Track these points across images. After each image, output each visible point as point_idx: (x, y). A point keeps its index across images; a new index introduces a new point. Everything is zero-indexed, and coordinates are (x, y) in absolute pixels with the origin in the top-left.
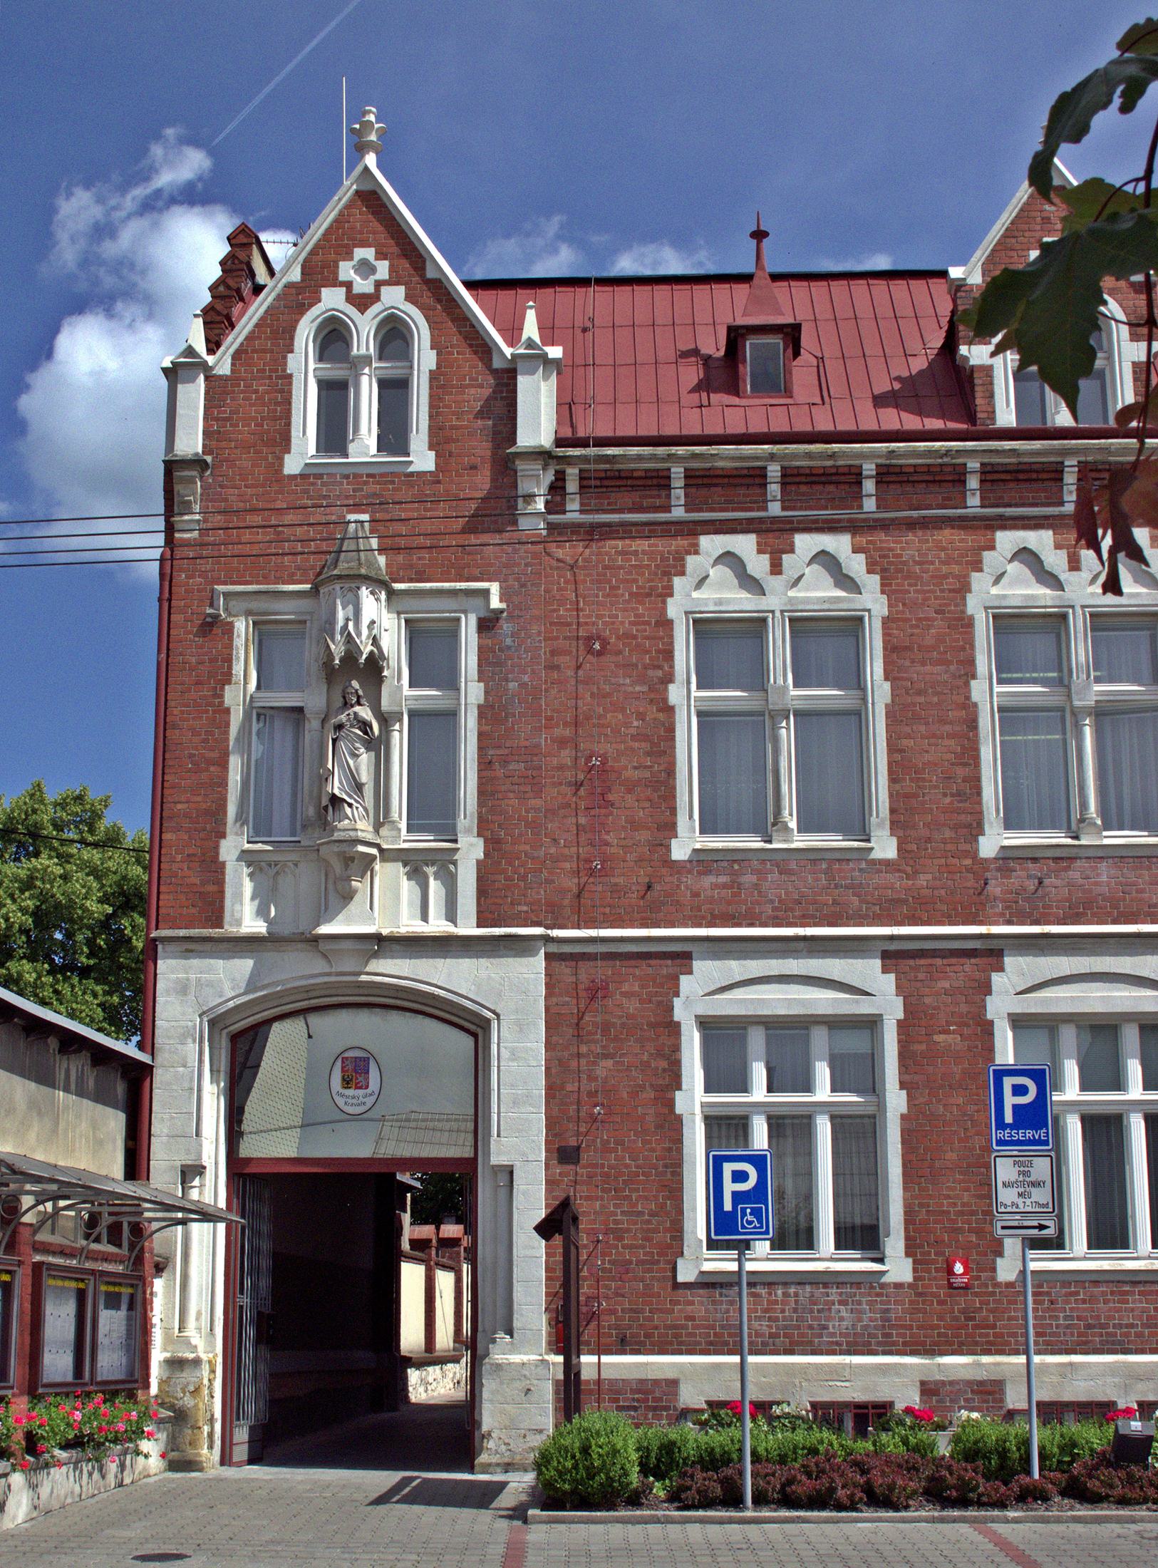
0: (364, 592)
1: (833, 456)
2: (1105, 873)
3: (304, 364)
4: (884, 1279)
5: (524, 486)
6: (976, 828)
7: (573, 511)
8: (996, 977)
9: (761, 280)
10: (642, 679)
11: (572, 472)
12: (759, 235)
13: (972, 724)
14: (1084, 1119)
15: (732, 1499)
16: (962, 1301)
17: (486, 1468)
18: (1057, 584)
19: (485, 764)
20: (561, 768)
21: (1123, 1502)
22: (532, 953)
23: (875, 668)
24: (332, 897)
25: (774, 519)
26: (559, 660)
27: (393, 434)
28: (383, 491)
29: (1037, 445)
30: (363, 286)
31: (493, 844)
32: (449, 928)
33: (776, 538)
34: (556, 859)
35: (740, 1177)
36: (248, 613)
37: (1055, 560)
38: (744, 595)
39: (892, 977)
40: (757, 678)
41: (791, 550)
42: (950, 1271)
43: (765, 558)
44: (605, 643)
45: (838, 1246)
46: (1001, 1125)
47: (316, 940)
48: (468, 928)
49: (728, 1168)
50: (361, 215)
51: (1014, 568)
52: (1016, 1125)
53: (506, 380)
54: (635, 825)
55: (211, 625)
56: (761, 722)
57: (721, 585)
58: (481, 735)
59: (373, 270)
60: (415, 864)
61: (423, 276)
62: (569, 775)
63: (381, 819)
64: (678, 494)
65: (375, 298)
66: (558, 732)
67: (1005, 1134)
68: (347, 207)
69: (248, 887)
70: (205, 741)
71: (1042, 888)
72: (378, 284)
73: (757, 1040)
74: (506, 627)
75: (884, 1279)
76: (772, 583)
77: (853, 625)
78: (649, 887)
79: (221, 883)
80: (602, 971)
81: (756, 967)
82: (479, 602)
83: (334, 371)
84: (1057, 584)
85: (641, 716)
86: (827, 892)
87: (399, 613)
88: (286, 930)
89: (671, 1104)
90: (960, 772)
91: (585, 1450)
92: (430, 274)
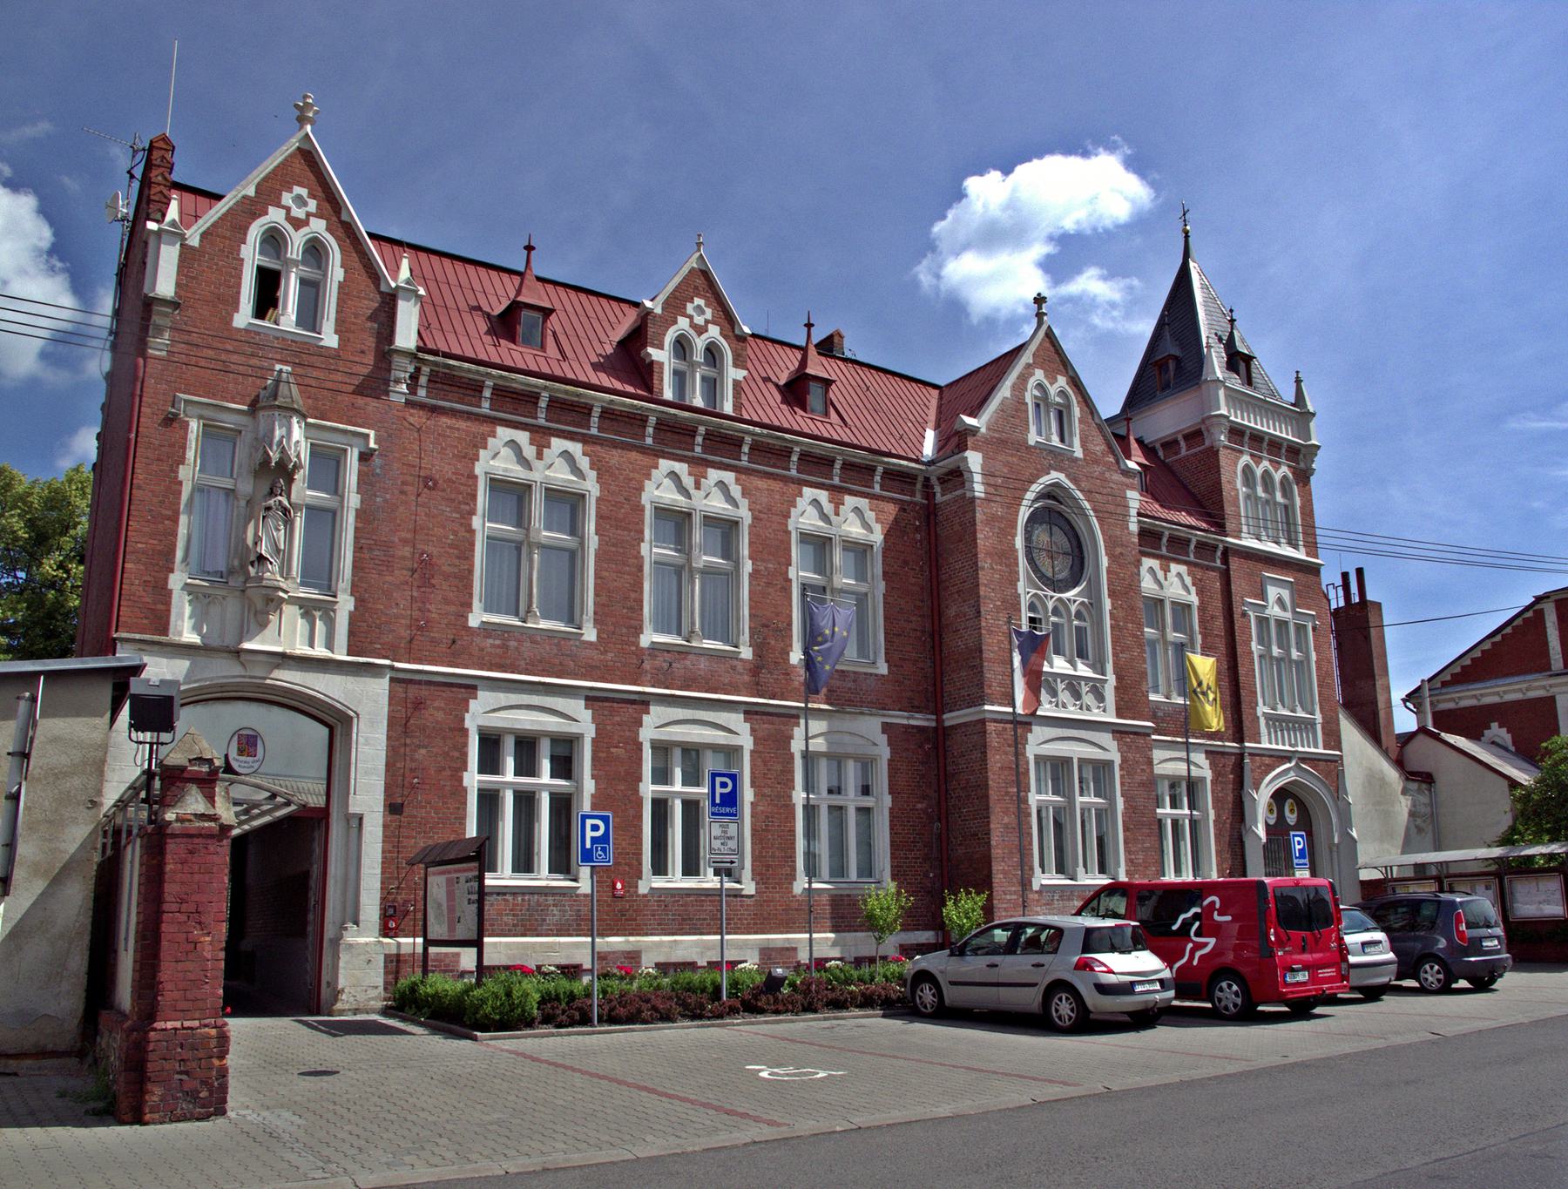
0: (295, 420)
1: (579, 395)
2: (703, 664)
3: (251, 255)
5: (395, 374)
6: (639, 630)
8: (645, 718)
10: (457, 510)
11: (426, 370)
12: (529, 248)
14: (515, 792)
15: (585, 1020)
16: (620, 905)
17: (341, 1012)
18: (689, 496)
19: (358, 548)
20: (404, 558)
21: (777, 1012)
22: (381, 676)
23: (591, 526)
24: (253, 626)
25: (592, 436)
26: (406, 488)
27: (310, 315)
28: (302, 353)
29: (687, 414)
30: (298, 213)
31: (360, 602)
32: (308, 652)
33: (541, 437)
34: (396, 617)
35: (724, 785)
36: (200, 417)
37: (688, 481)
38: (519, 468)
40: (521, 519)
41: (657, 468)
42: (614, 887)
43: (692, 479)
44: (436, 483)
47: (238, 653)
49: (589, 822)
50: (300, 166)
51: (667, 482)
53: (389, 301)
54: (447, 601)
55: (172, 420)
56: (518, 548)
57: (506, 459)
58: (356, 529)
59: (305, 204)
60: (308, 609)
62: (409, 564)
63: (286, 572)
64: (595, 420)
65: (306, 223)
66: (403, 535)
68: (291, 156)
69: (188, 610)
70: (162, 502)
71: (674, 669)
72: (308, 215)
73: (677, 754)
74: (377, 461)
76: (536, 464)
78: (454, 642)
79: (168, 604)
80: (424, 692)
81: (515, 698)
82: (360, 441)
83: (682, 366)
84: (689, 496)
85: (455, 533)
86: (557, 657)
88: (215, 642)
89: (461, 780)
90: (633, 595)
91: (509, 994)
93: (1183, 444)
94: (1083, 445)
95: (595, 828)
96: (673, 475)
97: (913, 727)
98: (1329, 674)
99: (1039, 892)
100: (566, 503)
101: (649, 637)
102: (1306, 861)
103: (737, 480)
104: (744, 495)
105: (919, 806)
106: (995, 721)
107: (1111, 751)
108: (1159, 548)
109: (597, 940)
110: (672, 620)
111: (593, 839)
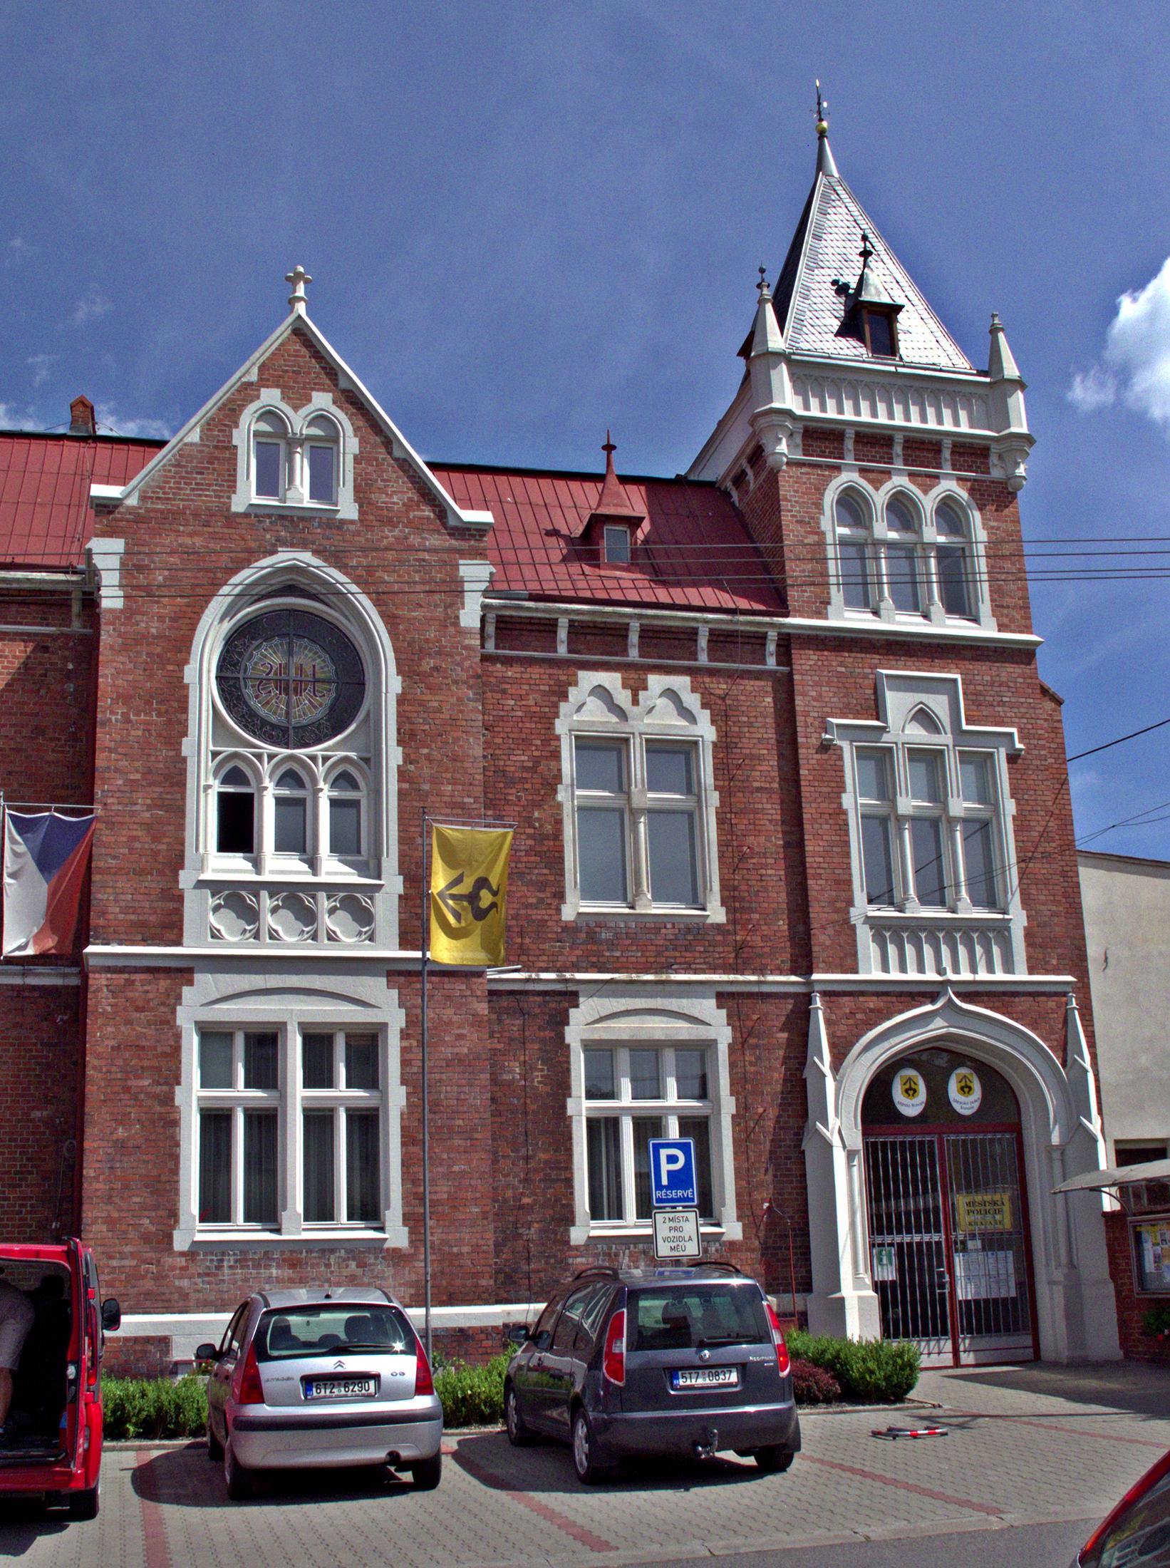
4: (386, 1246)
7: (490, 647)
9: (612, 481)
12: (609, 448)
13: (844, 828)
14: (681, 1119)
35: (673, 1159)
38: (684, 723)
39: (724, 1012)
40: (621, 784)
43: (628, 693)
46: (659, 1186)
49: (664, 1153)
52: (667, 1188)
56: (623, 815)
61: (390, 453)
67: (662, 1194)
73: (623, 1058)
75: (386, 1246)
77: (687, 748)
87: (851, 741)
93: (750, 472)
94: (361, 494)
96: (601, 692)
97: (34, 988)
98: (73, 809)
100: (672, 754)
101: (575, 906)
102: (694, 1192)
104: (704, 706)
105: (36, 1114)
106: (109, 970)
107: (386, 1008)
108: (624, 652)
109: (434, 1311)
110: (611, 880)
111: (669, 1172)
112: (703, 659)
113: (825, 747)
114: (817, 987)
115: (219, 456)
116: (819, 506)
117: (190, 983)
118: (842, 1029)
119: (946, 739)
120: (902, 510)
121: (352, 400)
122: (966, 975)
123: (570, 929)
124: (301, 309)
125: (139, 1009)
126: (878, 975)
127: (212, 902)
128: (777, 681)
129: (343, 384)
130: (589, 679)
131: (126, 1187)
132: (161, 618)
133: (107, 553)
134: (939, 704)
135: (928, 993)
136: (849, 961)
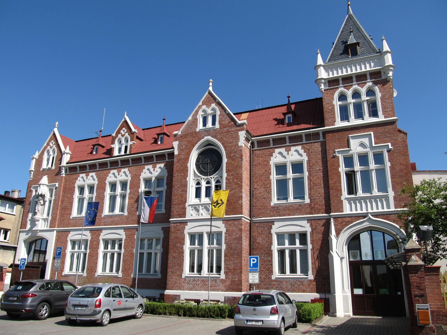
18: (285, 157)
45: (290, 273)
48: (49, 229)
49: (252, 259)
65: (124, 135)
67: (251, 269)
84: (285, 157)
92: (227, 112)
95: (254, 261)
99: (185, 279)
103: (129, 170)
109: (210, 292)
112: (304, 142)
113: (334, 157)
114: (332, 217)
115: (195, 121)
116: (333, 99)
117: (187, 225)
118: (339, 227)
119: (368, 149)
120: (356, 95)
121: (219, 104)
122: (375, 210)
123: (273, 207)
124: (211, 89)
125: (178, 231)
126: (349, 212)
127: (191, 209)
128: (326, 144)
129: (217, 101)
130: (277, 151)
131: (175, 265)
132: (184, 155)
133: (176, 144)
134: (366, 141)
135: (364, 216)
136: (341, 209)
